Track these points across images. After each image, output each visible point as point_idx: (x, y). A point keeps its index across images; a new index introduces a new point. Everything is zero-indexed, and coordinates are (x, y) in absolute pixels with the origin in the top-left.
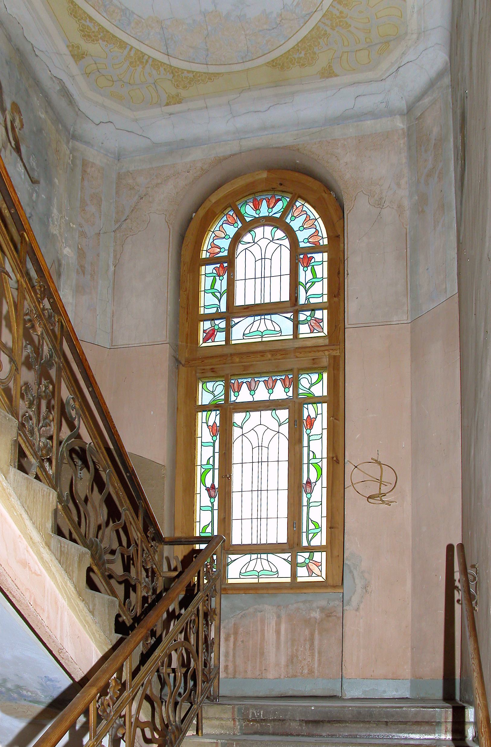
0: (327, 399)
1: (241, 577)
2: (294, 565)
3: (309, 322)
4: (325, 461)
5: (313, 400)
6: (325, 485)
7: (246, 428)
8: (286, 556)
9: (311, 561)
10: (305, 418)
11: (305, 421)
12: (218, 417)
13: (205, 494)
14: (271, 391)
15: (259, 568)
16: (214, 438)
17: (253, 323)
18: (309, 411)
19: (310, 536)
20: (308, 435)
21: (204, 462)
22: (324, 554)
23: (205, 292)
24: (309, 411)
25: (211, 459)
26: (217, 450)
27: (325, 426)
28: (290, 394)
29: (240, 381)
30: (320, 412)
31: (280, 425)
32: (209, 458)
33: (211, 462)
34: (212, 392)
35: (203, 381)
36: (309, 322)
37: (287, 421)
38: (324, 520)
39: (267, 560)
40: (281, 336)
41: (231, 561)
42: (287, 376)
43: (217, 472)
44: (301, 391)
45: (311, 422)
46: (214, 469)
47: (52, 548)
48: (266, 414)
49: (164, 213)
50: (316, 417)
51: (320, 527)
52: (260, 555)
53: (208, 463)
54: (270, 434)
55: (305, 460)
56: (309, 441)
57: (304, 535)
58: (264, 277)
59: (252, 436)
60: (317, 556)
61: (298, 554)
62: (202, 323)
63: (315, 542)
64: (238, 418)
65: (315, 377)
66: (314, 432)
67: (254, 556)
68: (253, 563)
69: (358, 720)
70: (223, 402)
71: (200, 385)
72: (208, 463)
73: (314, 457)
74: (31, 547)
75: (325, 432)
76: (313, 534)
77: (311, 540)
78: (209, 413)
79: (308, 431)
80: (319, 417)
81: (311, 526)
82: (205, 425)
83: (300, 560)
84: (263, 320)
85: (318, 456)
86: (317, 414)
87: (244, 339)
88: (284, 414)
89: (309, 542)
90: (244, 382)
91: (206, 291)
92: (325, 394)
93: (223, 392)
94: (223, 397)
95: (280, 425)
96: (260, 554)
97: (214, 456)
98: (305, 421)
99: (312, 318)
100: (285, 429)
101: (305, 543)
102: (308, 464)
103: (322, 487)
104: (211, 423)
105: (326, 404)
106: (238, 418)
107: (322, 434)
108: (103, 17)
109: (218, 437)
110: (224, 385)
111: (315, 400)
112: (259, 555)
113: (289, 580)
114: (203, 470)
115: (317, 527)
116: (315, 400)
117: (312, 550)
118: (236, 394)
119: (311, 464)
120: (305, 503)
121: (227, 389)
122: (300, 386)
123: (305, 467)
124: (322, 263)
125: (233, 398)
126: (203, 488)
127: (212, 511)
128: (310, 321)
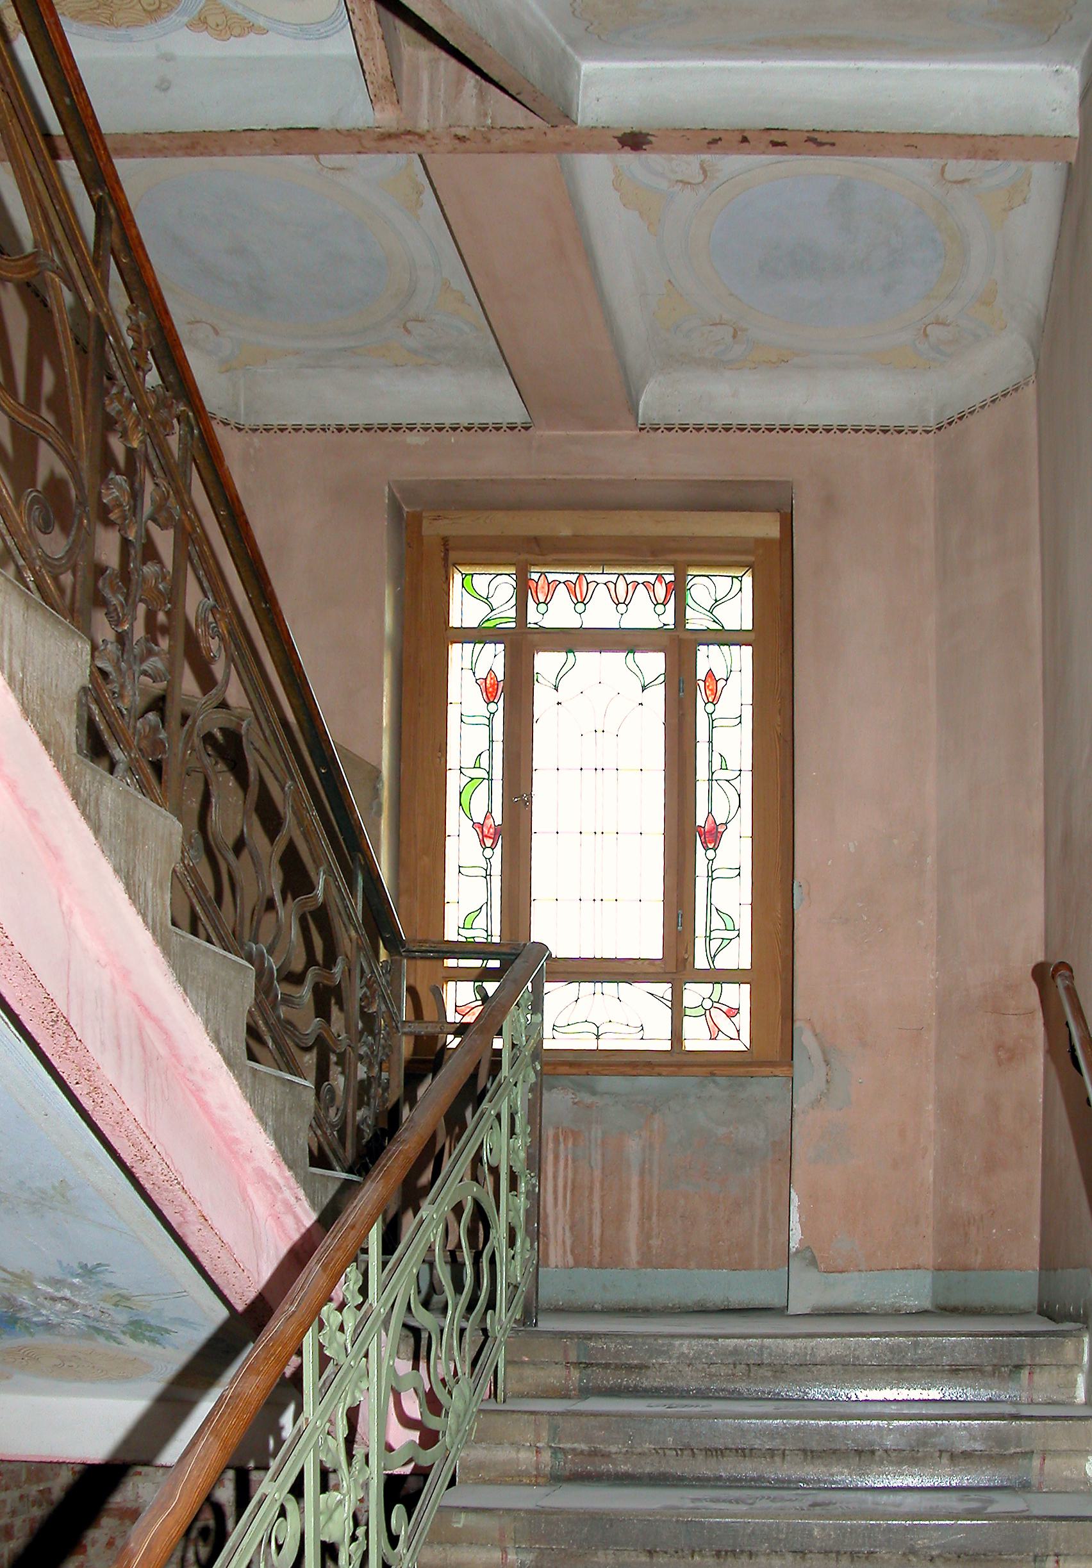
0: (752, 636)
3: (707, 1012)
4: (747, 778)
5: (720, 637)
9: (715, 1005)
11: (702, 684)
14: (622, 608)
16: (492, 707)
18: (709, 659)
19: (715, 945)
20: (710, 714)
21: (469, 762)
24: (709, 659)
25: (485, 756)
26: (498, 734)
28: (669, 618)
29: (551, 577)
30: (736, 668)
35: (463, 572)
42: (660, 577)
45: (713, 836)
47: (106, 818)
49: (372, 63)
53: (477, 765)
56: (712, 727)
62: (451, 984)
63: (724, 961)
64: (546, 663)
65: (723, 584)
66: (721, 709)
69: (819, 1367)
70: (513, 625)
71: (458, 577)
72: (477, 765)
73: (724, 767)
74: (56, 602)
75: (748, 713)
77: (715, 956)
78: (479, 646)
79: (710, 708)
81: (717, 922)
88: (654, 663)
90: (560, 582)
92: (748, 625)
93: (513, 601)
97: (490, 750)
98: (702, 684)
99: (715, 1005)
101: (701, 962)
102: (710, 780)
104: (482, 673)
105: (750, 648)
107: (740, 716)
109: (501, 703)
111: (724, 638)
113: (667, 1046)
115: (730, 927)
116: (724, 638)
118: (542, 607)
121: (523, 590)
122: (689, 601)
125: (533, 617)
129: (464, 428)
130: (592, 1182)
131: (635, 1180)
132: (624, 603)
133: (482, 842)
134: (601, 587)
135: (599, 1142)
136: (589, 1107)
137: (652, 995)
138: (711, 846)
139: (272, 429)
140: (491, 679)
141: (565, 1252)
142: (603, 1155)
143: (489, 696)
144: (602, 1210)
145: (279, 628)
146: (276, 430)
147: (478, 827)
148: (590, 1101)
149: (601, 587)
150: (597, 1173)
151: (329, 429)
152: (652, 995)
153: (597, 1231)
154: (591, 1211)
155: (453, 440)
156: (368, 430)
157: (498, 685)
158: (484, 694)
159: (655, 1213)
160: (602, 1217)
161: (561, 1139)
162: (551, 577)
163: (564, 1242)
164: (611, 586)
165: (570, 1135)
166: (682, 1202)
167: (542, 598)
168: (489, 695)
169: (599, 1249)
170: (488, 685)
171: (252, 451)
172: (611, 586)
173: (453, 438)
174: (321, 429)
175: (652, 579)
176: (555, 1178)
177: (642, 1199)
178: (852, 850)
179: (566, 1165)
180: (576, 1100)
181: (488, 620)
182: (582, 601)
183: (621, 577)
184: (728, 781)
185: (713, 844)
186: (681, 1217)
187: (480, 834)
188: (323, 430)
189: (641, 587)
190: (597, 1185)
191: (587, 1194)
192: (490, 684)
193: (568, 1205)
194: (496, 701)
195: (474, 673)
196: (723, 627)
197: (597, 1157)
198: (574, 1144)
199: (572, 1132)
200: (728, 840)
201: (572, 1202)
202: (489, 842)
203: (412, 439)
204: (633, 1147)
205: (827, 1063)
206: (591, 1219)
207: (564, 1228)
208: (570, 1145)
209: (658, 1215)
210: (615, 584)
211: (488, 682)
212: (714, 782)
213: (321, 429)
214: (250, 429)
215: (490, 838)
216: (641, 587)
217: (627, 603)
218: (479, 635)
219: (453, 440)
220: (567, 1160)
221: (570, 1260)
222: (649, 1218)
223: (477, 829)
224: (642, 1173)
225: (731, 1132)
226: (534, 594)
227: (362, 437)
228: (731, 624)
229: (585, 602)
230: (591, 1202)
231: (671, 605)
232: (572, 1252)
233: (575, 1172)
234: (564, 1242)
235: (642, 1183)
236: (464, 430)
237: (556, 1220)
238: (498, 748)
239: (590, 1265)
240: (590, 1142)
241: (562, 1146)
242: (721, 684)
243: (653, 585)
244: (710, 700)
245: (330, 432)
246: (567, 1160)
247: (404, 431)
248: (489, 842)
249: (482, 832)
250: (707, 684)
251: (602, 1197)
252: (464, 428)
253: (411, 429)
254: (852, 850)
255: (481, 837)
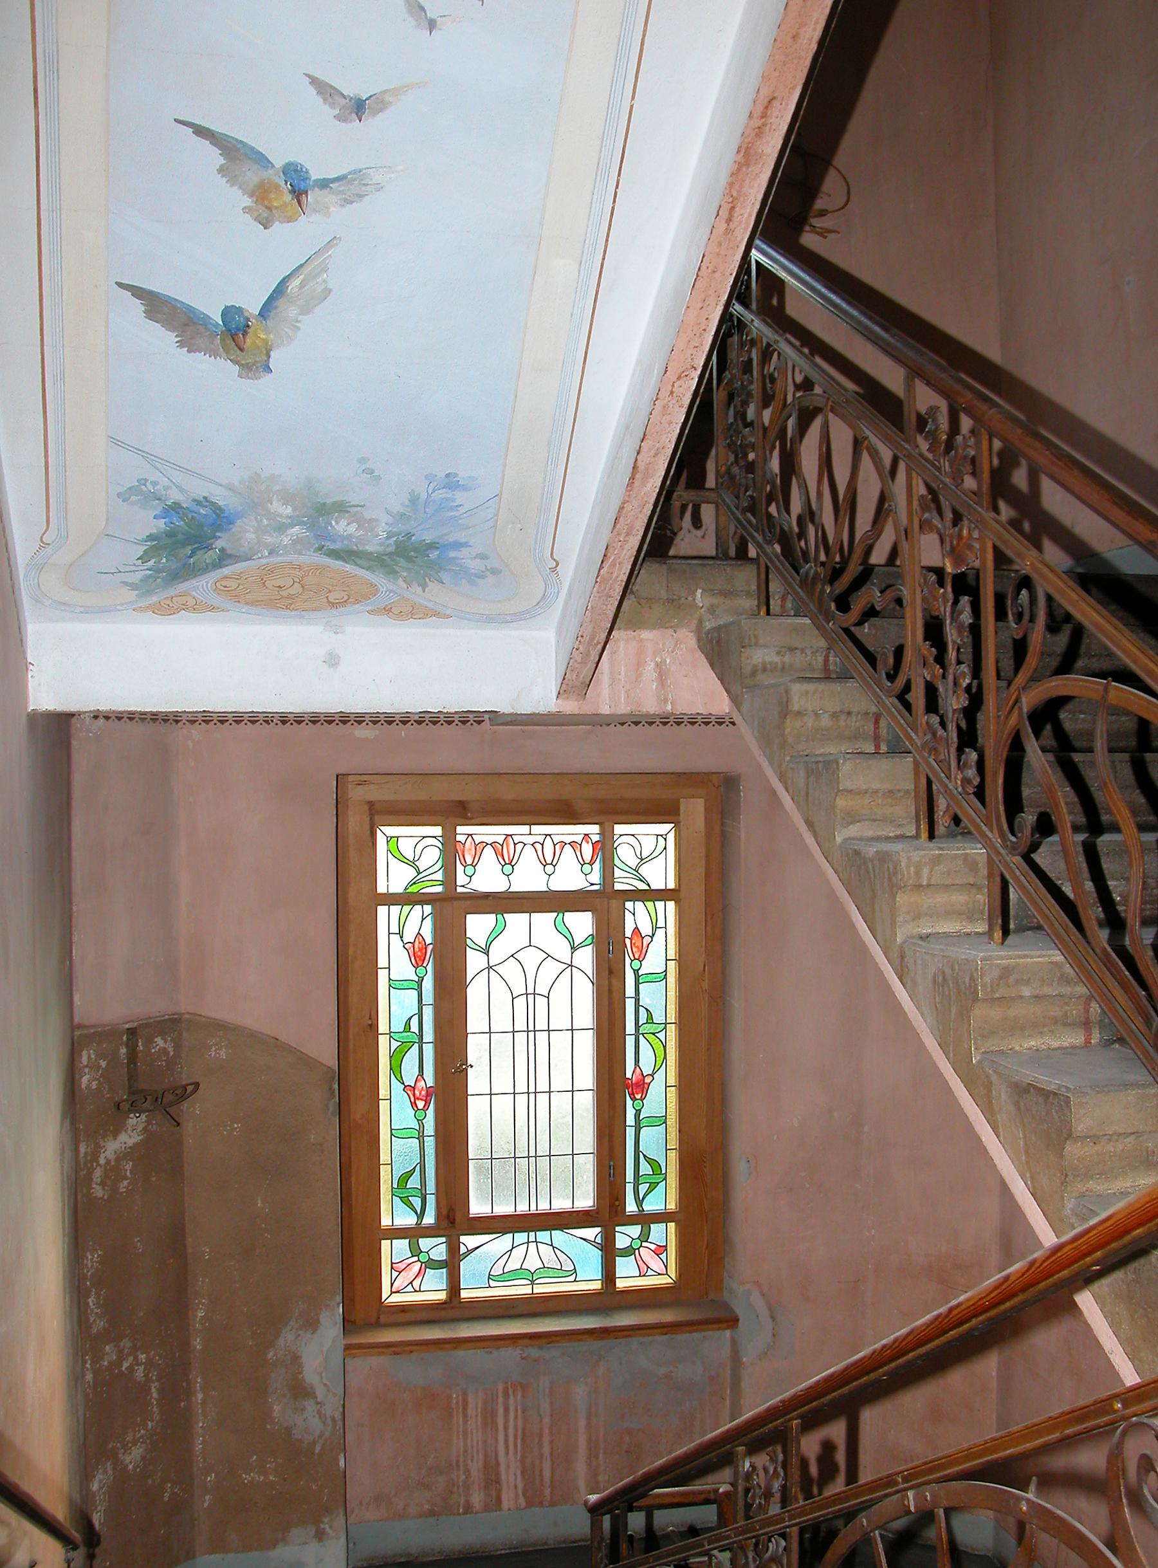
1: (492, 1283)
2: (609, 1252)
3: (637, 1251)
4: (672, 1030)
6: (672, 1081)
7: (498, 952)
8: (592, 1233)
10: (628, 933)
12: (428, 922)
13: (401, 1099)
14: (549, 869)
15: (533, 1263)
16: (421, 971)
17: (511, 1250)
18: (638, 916)
19: (643, 1189)
20: (636, 972)
21: (398, 1026)
22: (672, 1226)
23: (391, 1037)
27: (672, 954)
28: (596, 877)
30: (661, 923)
31: (574, 949)
32: (410, 1019)
33: (415, 1027)
34: (413, 863)
36: (637, 1251)
37: (589, 941)
38: (673, 1155)
39: (552, 1245)
40: (575, 1281)
41: (468, 1251)
43: (429, 1050)
44: (617, 873)
45: (641, 1087)
46: (421, 1042)
48: (544, 921)
50: (653, 935)
51: (664, 1172)
52: (534, 1233)
54: (551, 969)
55: (630, 1028)
57: (629, 1188)
58: (535, 1031)
59: (511, 970)
60: (658, 1231)
61: (617, 1229)
64: (478, 926)
67: (521, 1237)
68: (519, 1252)
75: (672, 965)
76: (648, 1185)
77: (643, 1199)
78: (407, 908)
79: (636, 964)
80: (660, 933)
81: (645, 1168)
82: (395, 939)
83: (621, 1242)
84: (532, 1246)
85: (658, 1017)
86: (655, 928)
87: (490, 1287)
88: (582, 923)
89: (639, 1202)
91: (392, 1034)
94: (439, 876)
95: (574, 949)
96: (535, 1231)
98: (628, 941)
100: (585, 958)
101: (631, 1207)
103: (667, 960)
104: (409, 936)
106: (478, 926)
108: (60, 74)
109: (430, 968)
110: (440, 845)
112: (532, 1234)
114: (395, 1044)
117: (645, 1220)
119: (643, 1034)
120: (630, 1119)
121: (450, 853)
122: (617, 862)
123: (630, 1042)
124: (665, 1028)
125: (461, 879)
126: (397, 1086)
127: (421, 1137)
128: (638, 1249)
129: (415, 721)
130: (541, 1429)
131: (582, 1423)
132: (551, 864)
133: (414, 1105)
134: (528, 848)
135: (547, 1391)
136: (537, 1360)
137: (584, 1239)
138: (638, 1097)
139: (212, 720)
140: (420, 943)
141: (517, 1496)
142: (551, 1403)
143: (418, 959)
144: (551, 1454)
145: (831, 1516)
146: (215, 721)
147: (410, 1089)
148: (537, 1355)
149: (528, 848)
150: (547, 1420)
151: (272, 721)
152: (584, 1239)
153: (547, 1474)
154: (541, 1456)
155: (403, 734)
156: (314, 722)
157: (426, 948)
158: (413, 959)
159: (602, 1451)
160: (552, 1460)
161: (511, 1392)
162: (478, 839)
163: (516, 1487)
164: (539, 847)
165: (519, 1388)
166: (627, 1439)
167: (469, 861)
168: (418, 959)
169: (549, 1490)
170: (417, 949)
171: (190, 744)
172: (539, 847)
173: (403, 731)
174: (264, 721)
175: (579, 839)
176: (506, 1428)
177: (589, 1440)
178: (796, 1125)
179: (516, 1417)
180: (524, 1356)
181: (414, 883)
182: (508, 864)
183: (548, 837)
184: (654, 1034)
185: (640, 1095)
186: (626, 1452)
187: (412, 1096)
188: (267, 722)
189: (568, 848)
190: (547, 1431)
191: (536, 1440)
192: (419, 948)
193: (519, 1452)
194: (425, 965)
195: (401, 937)
196: (649, 885)
197: (545, 1407)
198: (523, 1396)
199: (521, 1384)
200: (656, 1090)
201: (523, 1448)
202: (421, 1104)
203: (361, 732)
204: (580, 1393)
205: (773, 1318)
206: (541, 1463)
207: (515, 1474)
208: (519, 1397)
209: (605, 1453)
210: (542, 845)
211: (416, 946)
212: (641, 1036)
213: (264, 721)
214: (188, 721)
215: (421, 1099)
216: (568, 848)
217: (554, 864)
218: (408, 899)
219: (403, 734)
220: (516, 1411)
221: (522, 1501)
222: (597, 1456)
223: (409, 1092)
224: (589, 1418)
225: (671, 1372)
226: (461, 857)
227: (306, 730)
228: (657, 884)
229: (513, 864)
230: (541, 1446)
231: (597, 866)
232: (524, 1495)
233: (525, 1421)
234: (516, 1487)
235: (589, 1426)
236: (415, 723)
237: (508, 1467)
238: (428, 1013)
239: (541, 1504)
240: (538, 1392)
241: (512, 1399)
242: (646, 940)
243: (580, 845)
244: (637, 956)
245: (274, 724)
246: (516, 1411)
247: (352, 724)
248: (421, 1104)
249: (414, 1095)
250: (633, 941)
251: (552, 1442)
252: (415, 721)
253: (360, 722)
254: (796, 1125)
255: (412, 1100)
